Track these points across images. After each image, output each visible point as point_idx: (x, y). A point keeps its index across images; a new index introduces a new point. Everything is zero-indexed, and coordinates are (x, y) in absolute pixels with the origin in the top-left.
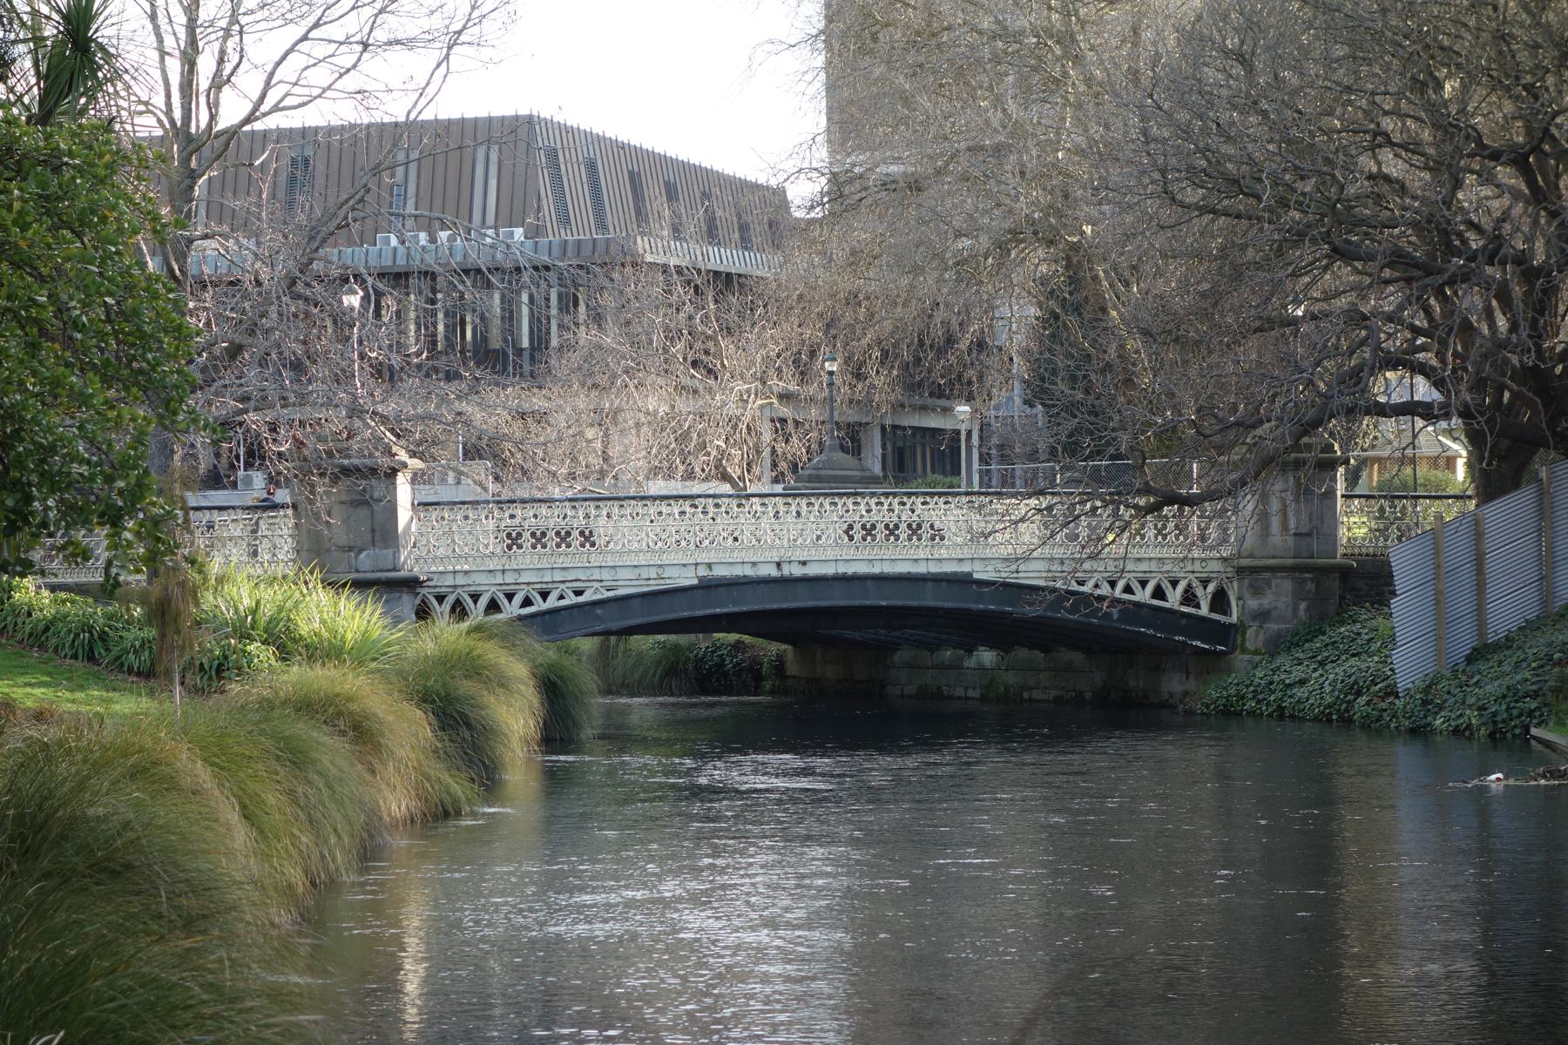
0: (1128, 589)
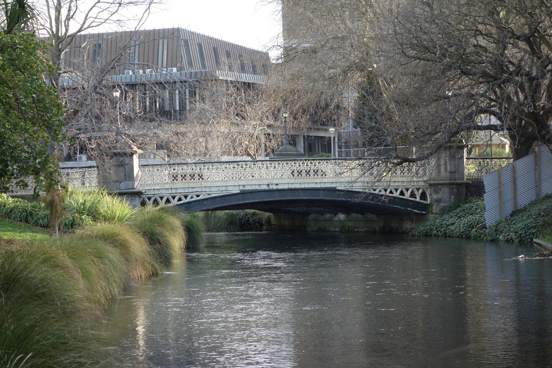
0: (391, 192)
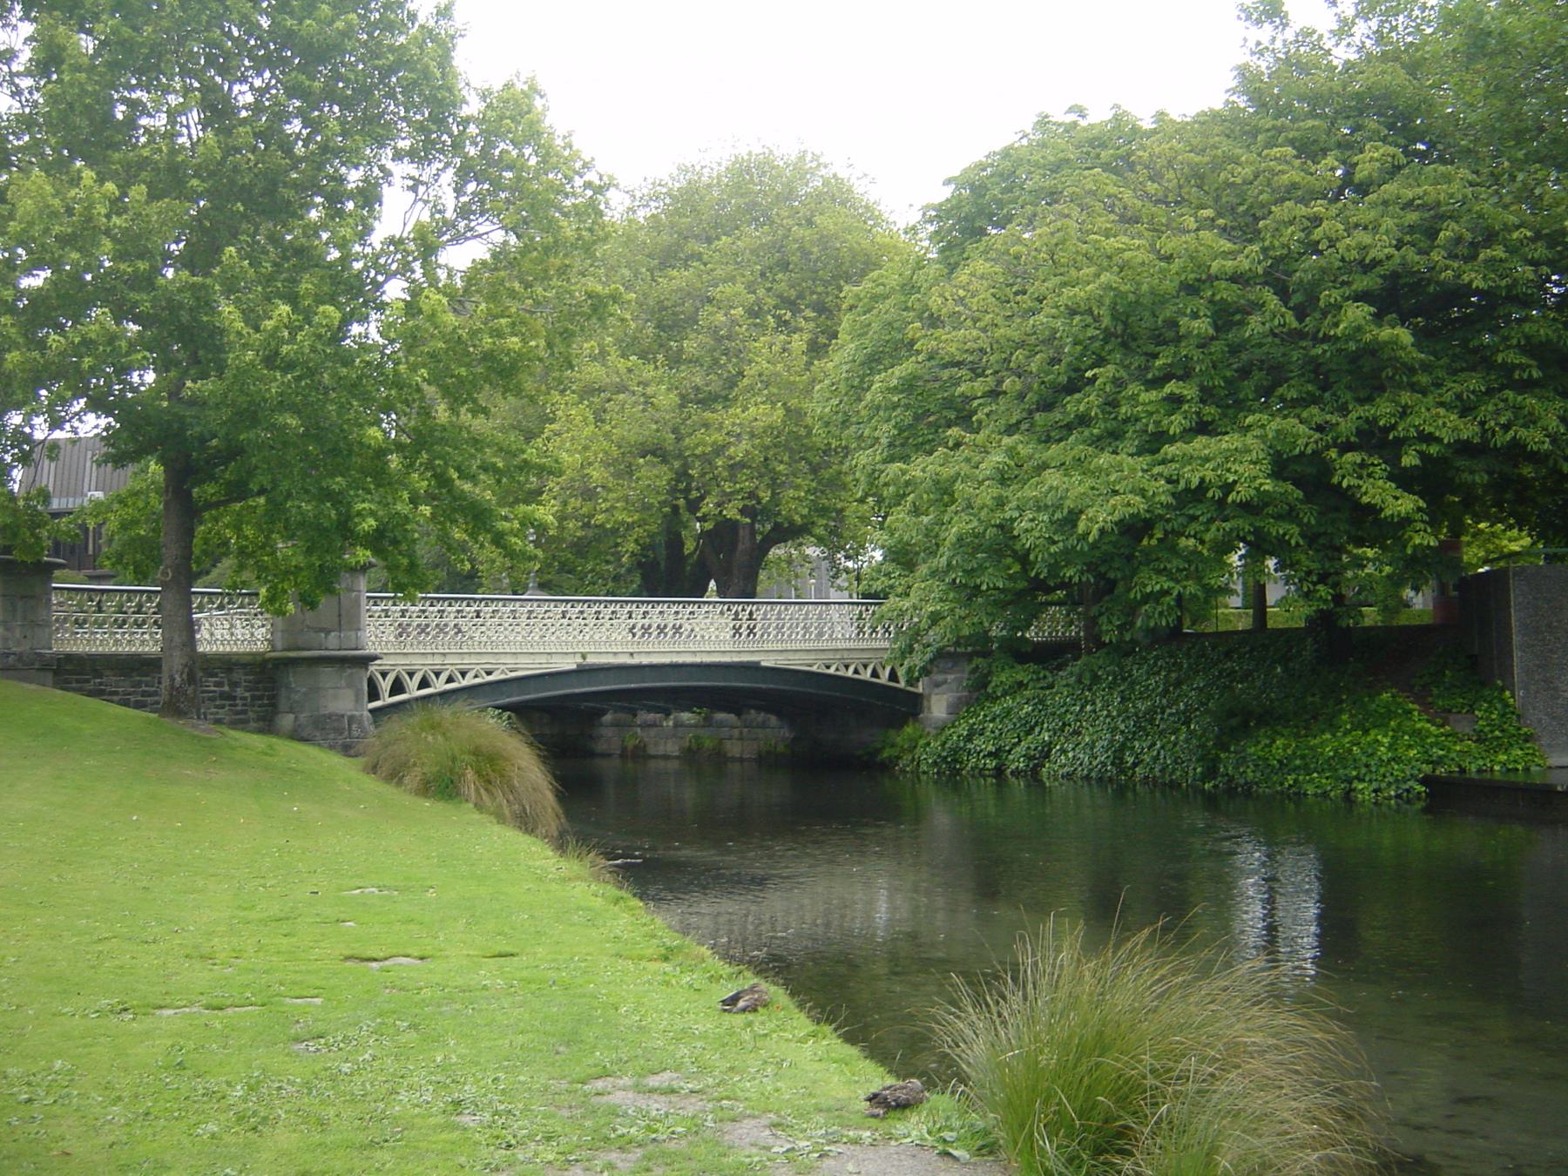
0: (856, 672)
